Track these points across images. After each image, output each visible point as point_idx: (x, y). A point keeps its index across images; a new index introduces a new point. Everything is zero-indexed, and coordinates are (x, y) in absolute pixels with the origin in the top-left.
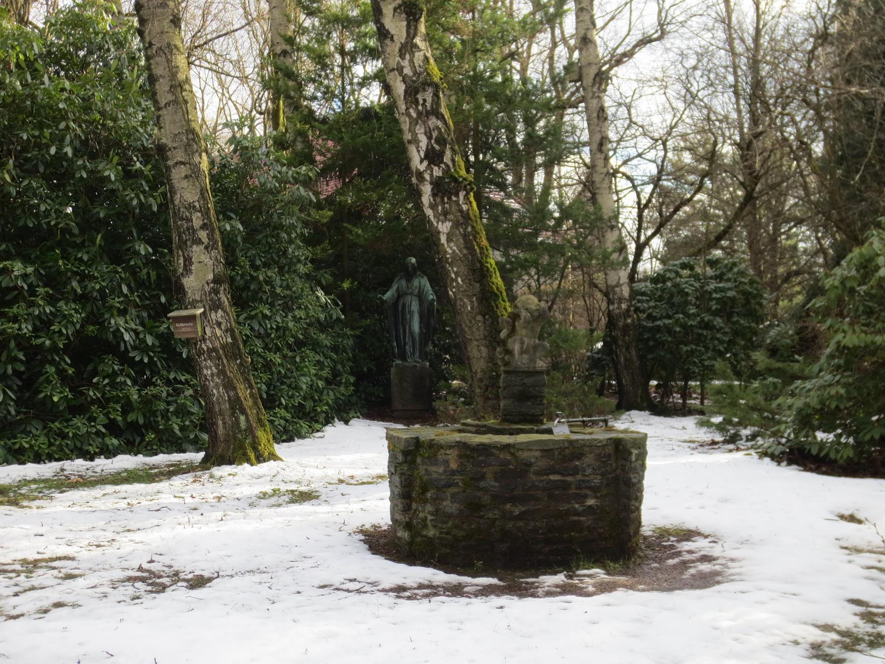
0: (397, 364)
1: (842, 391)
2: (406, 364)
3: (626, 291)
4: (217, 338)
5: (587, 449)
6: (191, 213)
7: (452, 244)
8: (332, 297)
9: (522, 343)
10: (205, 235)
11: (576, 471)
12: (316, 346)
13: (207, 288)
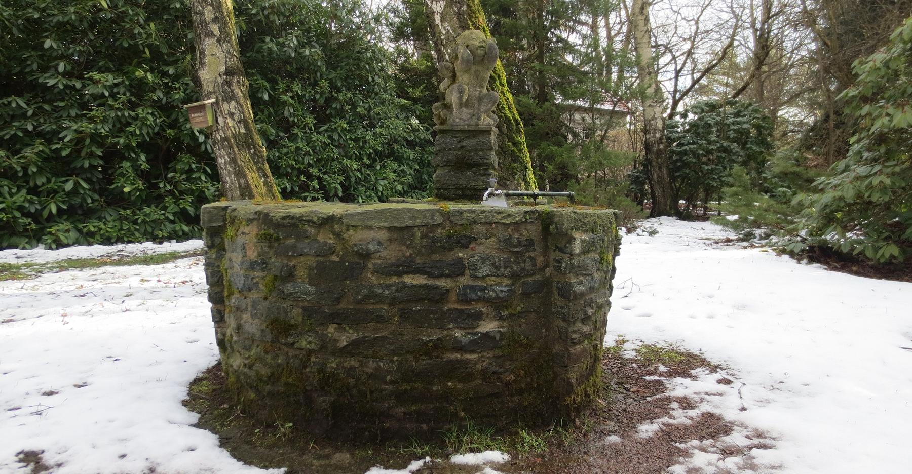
1: (888, 182)
3: (660, 124)
4: (229, 128)
5: (480, 229)
6: (203, 7)
7: (446, 24)
9: (461, 92)
10: (217, 29)
11: (458, 269)
12: (399, 159)
13: (220, 80)
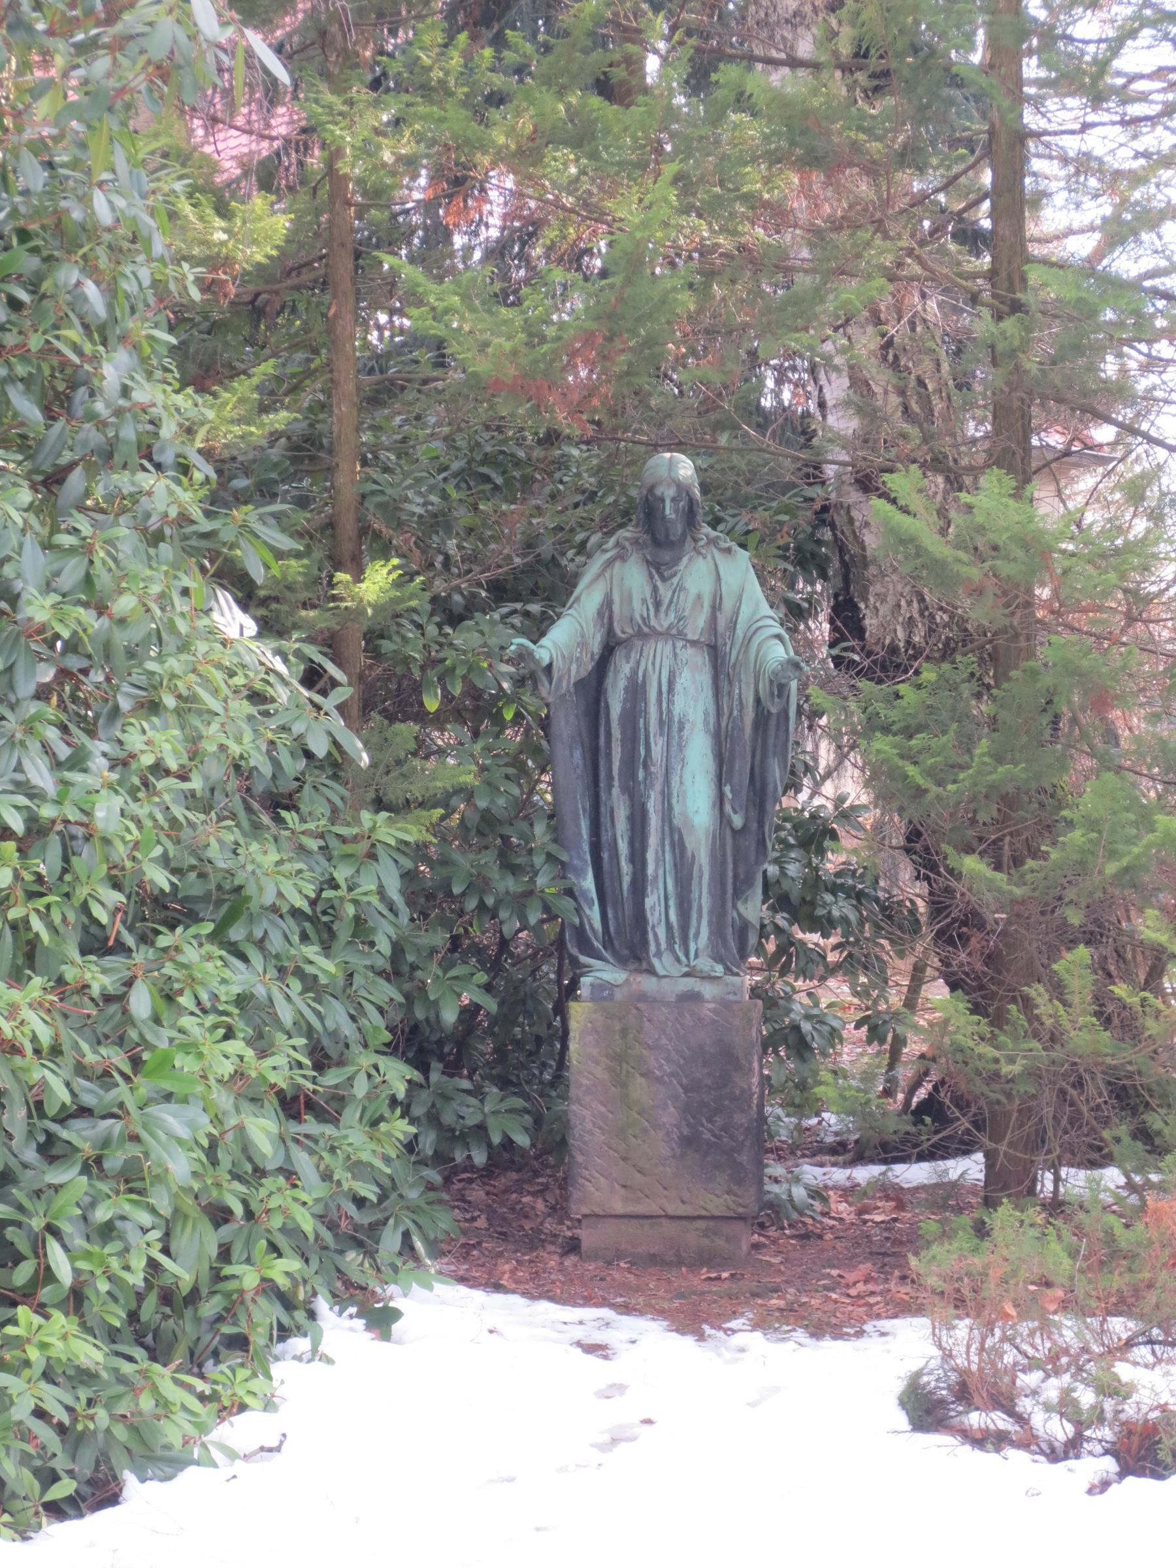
0: (602, 991)
2: (648, 984)
8: (291, 644)
